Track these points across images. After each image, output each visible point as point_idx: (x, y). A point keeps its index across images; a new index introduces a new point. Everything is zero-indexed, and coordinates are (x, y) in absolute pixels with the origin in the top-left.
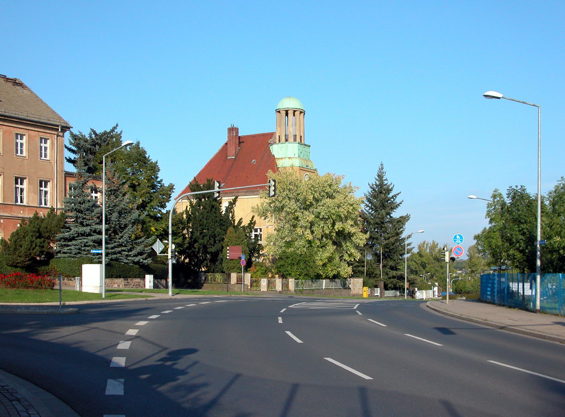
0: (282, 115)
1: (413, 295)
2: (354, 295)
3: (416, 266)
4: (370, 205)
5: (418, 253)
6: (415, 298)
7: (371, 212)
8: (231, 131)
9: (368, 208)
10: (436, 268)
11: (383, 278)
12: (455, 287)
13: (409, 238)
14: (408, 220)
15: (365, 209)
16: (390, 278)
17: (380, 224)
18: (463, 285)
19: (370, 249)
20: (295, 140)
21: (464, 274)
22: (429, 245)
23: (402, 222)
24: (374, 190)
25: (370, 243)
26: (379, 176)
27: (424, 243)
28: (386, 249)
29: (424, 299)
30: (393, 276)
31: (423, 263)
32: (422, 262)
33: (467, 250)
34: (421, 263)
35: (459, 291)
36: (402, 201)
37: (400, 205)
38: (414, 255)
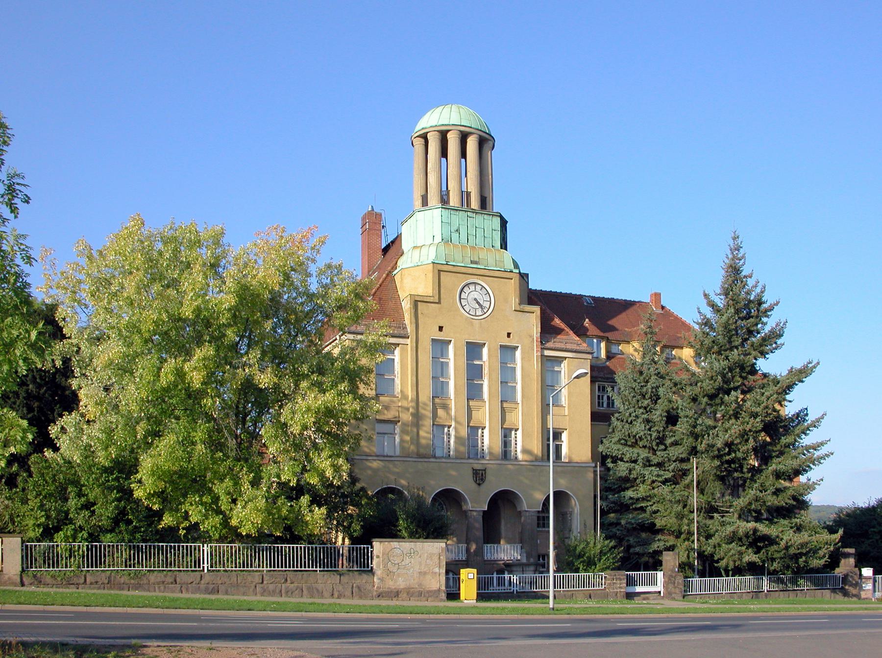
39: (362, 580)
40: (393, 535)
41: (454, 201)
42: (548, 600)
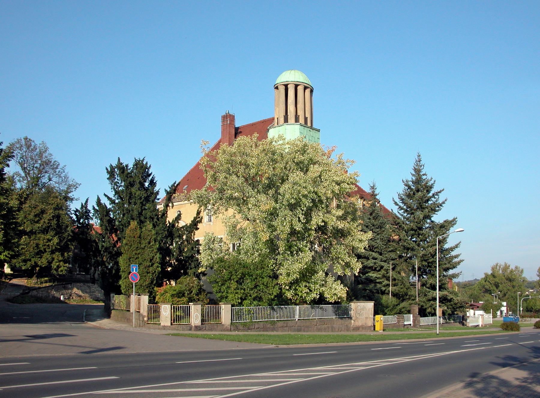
0: (280, 92)
1: (464, 321)
2: (357, 329)
3: (490, 286)
4: (405, 207)
5: (492, 274)
6: (466, 325)
7: (407, 216)
8: (225, 119)
9: (403, 211)
10: (508, 287)
11: (420, 301)
12: (525, 305)
13: (457, 247)
14: (455, 224)
15: (399, 213)
16: (430, 300)
17: (418, 230)
18: (533, 303)
19: (405, 263)
20: (297, 120)
21: (535, 293)
22: (502, 267)
23: (446, 227)
24: (409, 187)
25: (405, 255)
26: (415, 170)
27: (497, 265)
28: (424, 262)
29: (480, 326)
30: (433, 298)
31: (496, 283)
32: (495, 282)
33: (537, 270)
34: (494, 283)
35: (530, 309)
36: (446, 200)
37: (443, 205)
38: (488, 276)
39: (346, 322)
40: (150, 302)
41: (302, 120)
42: (505, 320)
